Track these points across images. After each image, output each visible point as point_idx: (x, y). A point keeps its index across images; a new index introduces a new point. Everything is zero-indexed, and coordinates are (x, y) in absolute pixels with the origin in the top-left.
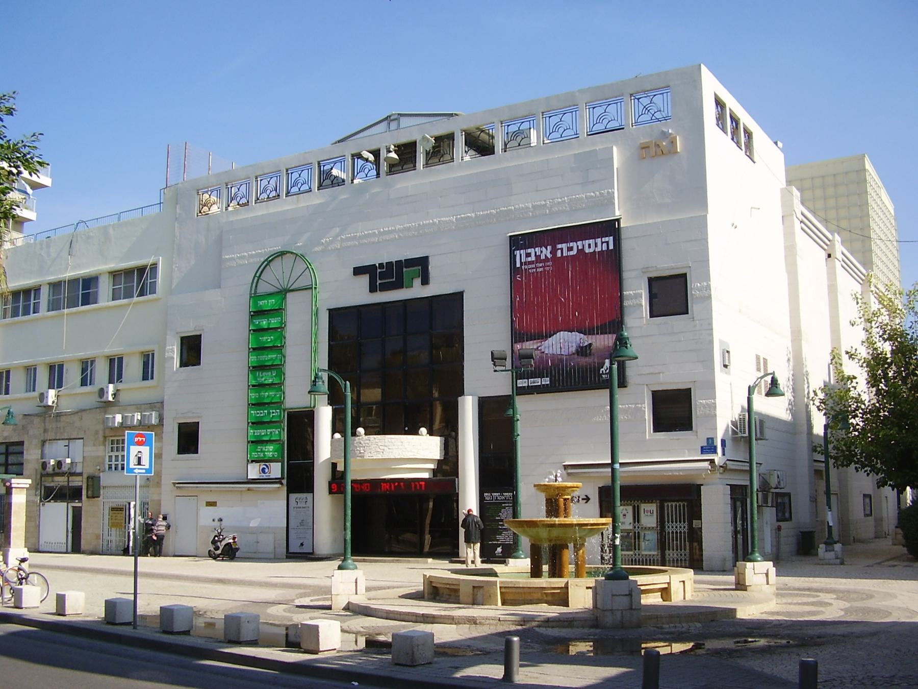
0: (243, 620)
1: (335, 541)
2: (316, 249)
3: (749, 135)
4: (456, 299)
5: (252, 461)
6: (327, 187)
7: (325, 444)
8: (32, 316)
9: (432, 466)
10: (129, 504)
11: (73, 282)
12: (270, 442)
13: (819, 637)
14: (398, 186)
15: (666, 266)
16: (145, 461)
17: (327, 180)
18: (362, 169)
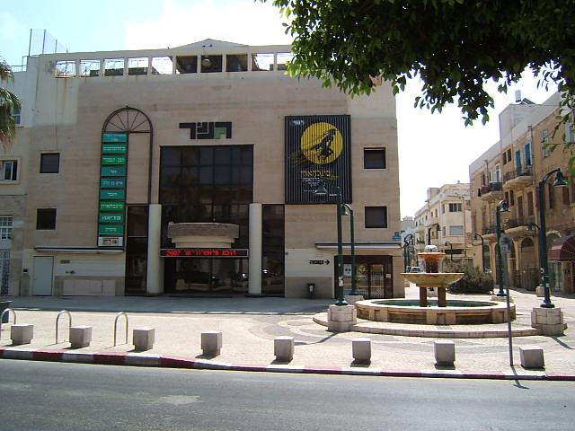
15: (373, 143)
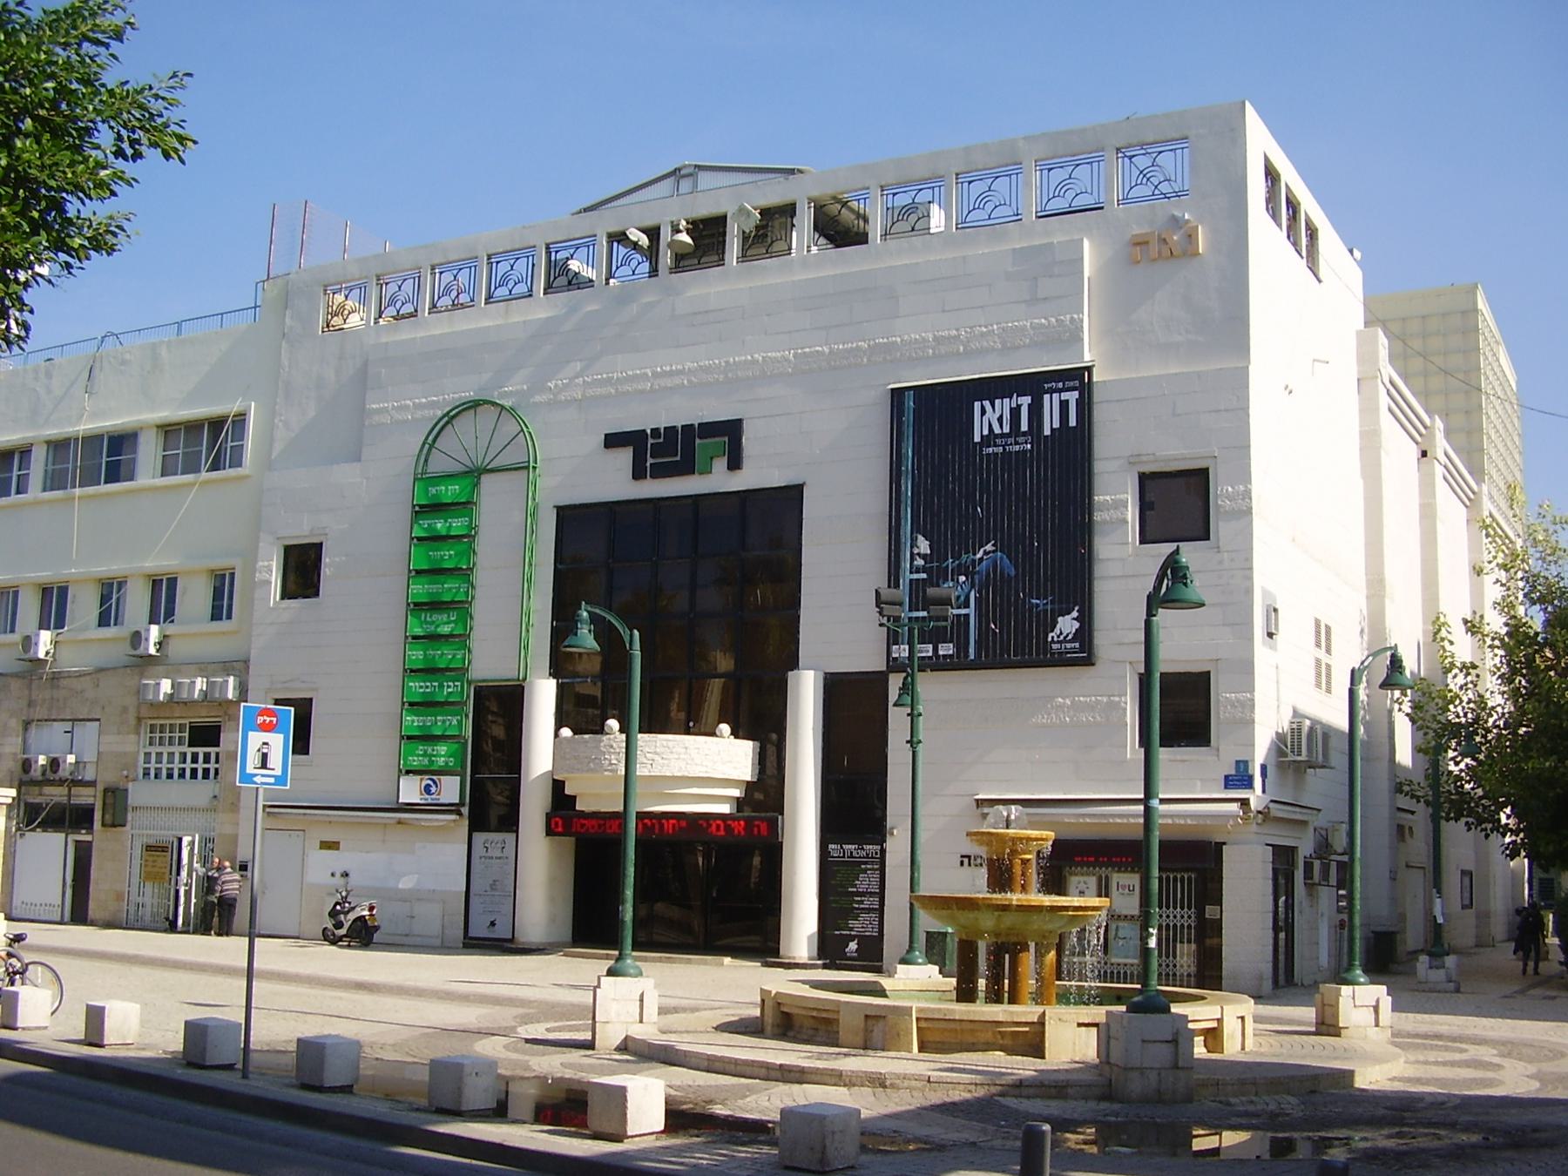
0: (467, 1070)
1: (552, 920)
2: (538, 398)
3: (1312, 233)
4: (791, 497)
5: (408, 772)
6: (559, 290)
7: (542, 743)
8: (14, 498)
9: (736, 793)
10: (180, 840)
11: (92, 440)
12: (443, 738)
13: (1535, 1130)
14: (691, 293)
15: (1172, 453)
16: (275, 761)
17: (561, 279)
18: (626, 261)
